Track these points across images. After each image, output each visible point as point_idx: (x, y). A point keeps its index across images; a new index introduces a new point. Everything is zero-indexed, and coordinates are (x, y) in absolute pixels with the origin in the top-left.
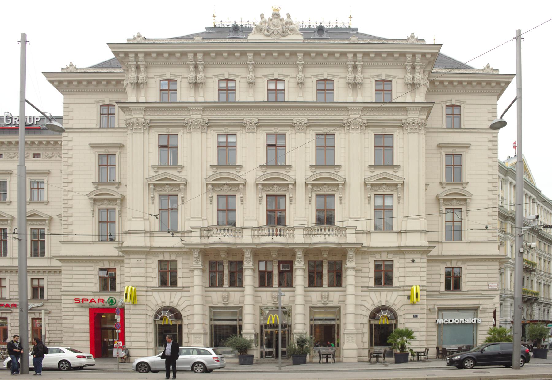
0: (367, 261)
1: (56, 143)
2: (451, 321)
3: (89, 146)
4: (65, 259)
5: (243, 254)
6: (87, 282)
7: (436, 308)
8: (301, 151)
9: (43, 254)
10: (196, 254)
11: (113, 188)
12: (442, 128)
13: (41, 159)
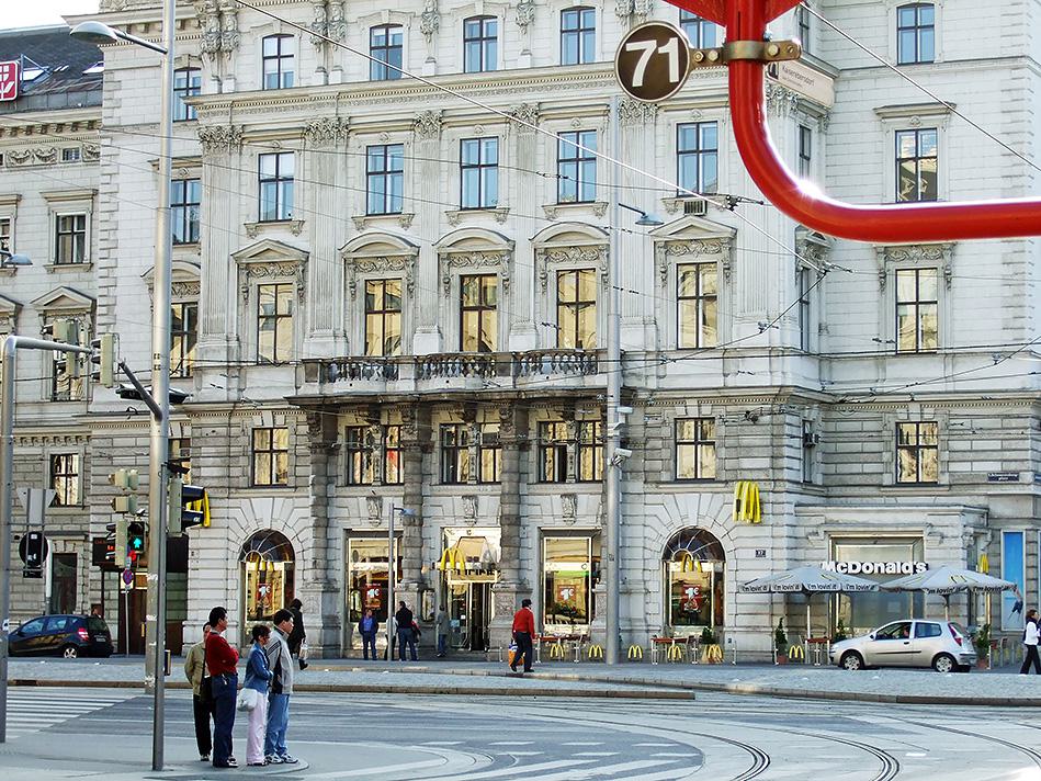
2: (854, 567)
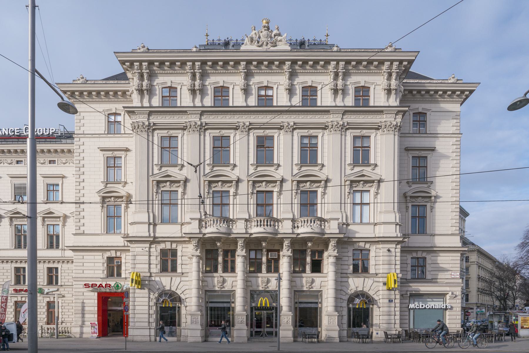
0: (346, 250)
1: (69, 151)
2: (422, 306)
3: (99, 150)
4: (75, 249)
5: (236, 243)
6: (95, 269)
7: (408, 293)
8: (286, 148)
9: (58, 247)
10: (194, 242)
11: (120, 186)
12: (409, 133)
13: (56, 164)
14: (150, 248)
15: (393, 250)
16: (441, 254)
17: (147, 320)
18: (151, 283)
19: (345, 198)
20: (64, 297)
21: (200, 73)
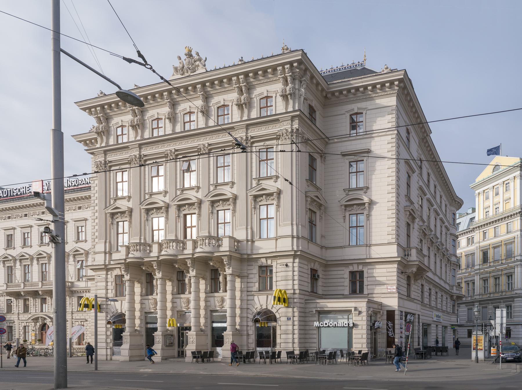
2: (326, 324)
14: (107, 274)
15: (290, 265)
16: (377, 266)
17: (104, 341)
18: (109, 307)
19: (252, 215)
20: (87, 321)
21: (290, 76)
